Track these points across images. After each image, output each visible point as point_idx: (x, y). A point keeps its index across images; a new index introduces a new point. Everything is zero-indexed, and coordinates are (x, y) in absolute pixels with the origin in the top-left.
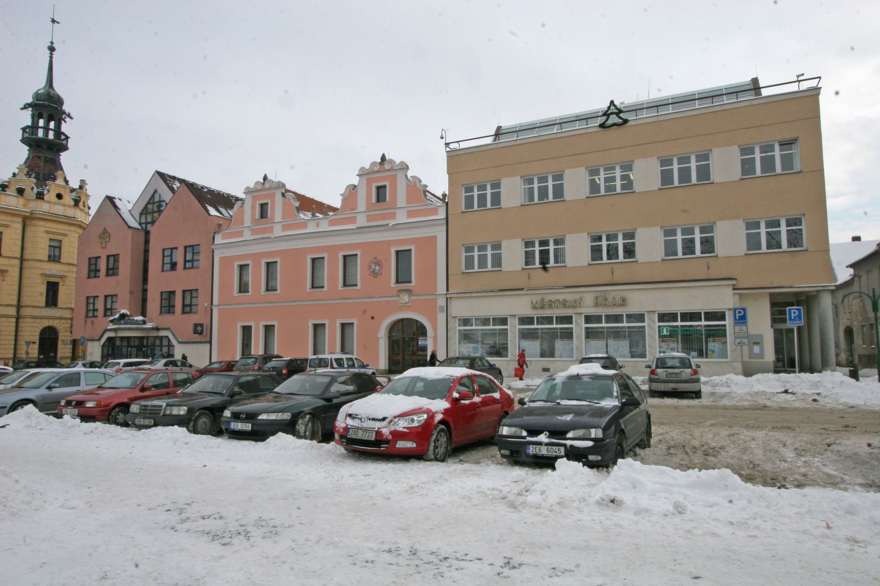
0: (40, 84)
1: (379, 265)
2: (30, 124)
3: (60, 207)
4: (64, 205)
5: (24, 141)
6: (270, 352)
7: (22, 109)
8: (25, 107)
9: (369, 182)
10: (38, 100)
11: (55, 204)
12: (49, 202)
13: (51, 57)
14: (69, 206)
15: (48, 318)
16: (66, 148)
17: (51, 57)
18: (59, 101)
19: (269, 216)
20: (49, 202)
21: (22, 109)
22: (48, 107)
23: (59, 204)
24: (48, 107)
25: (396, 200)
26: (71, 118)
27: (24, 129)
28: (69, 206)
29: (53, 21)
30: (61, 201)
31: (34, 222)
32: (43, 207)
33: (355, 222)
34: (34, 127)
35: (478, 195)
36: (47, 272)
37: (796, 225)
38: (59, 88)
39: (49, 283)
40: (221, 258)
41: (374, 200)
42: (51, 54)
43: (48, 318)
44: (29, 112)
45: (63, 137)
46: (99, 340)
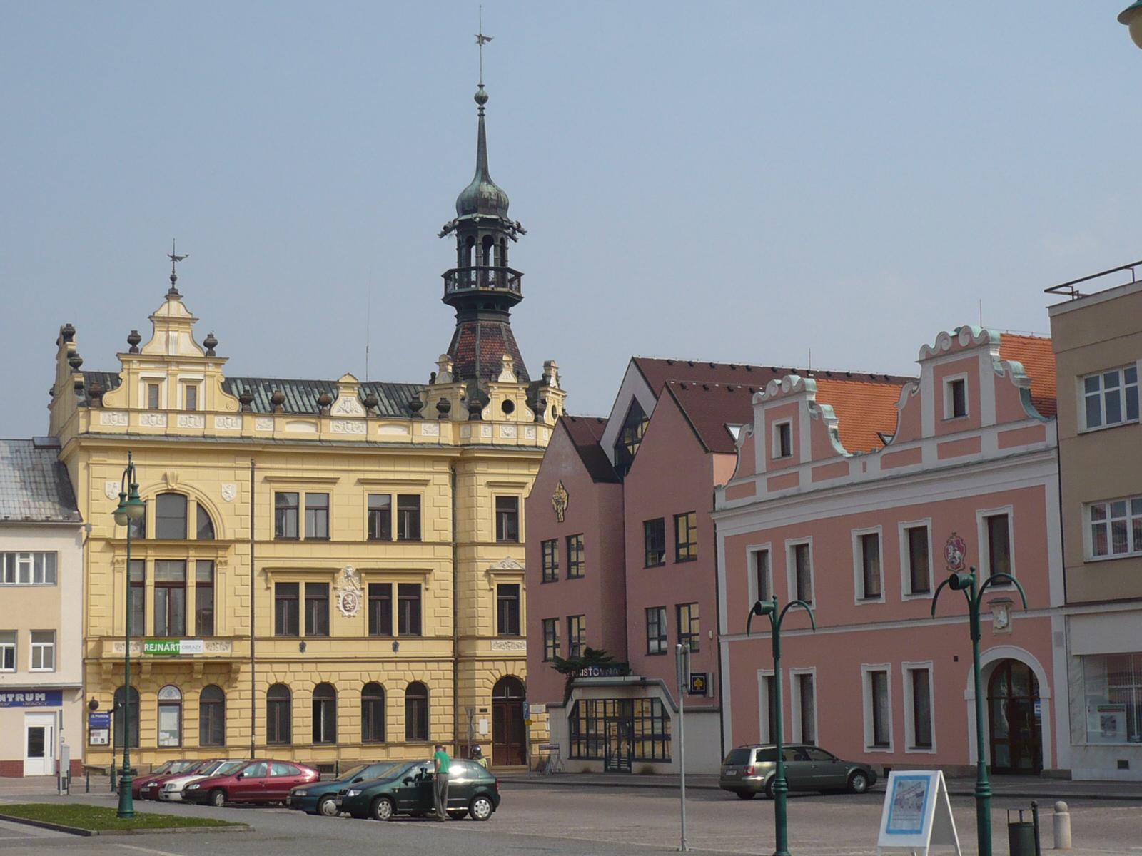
0: (463, 179)
1: (961, 550)
2: (456, 267)
3: (510, 430)
4: (516, 424)
5: (449, 299)
6: (598, 720)
7: (441, 236)
8: (447, 230)
9: (939, 373)
10: (465, 213)
11: (501, 423)
12: (491, 423)
13: (482, 115)
14: (526, 424)
15: (505, 660)
16: (515, 300)
17: (482, 115)
18: (500, 205)
19: (792, 452)
20: (491, 423)
21: (441, 236)
22: (482, 225)
23: (507, 423)
24: (482, 225)
25: (979, 416)
26: (523, 232)
27: (448, 276)
28: (526, 424)
29: (481, 39)
30: (512, 417)
31: (469, 467)
32: (483, 434)
33: (919, 460)
34: (464, 267)
35: (1107, 394)
36: (498, 567)
37: (1124, 532)
38: (503, 179)
39: (502, 589)
40: (726, 538)
41: (948, 411)
42: (482, 109)
43: (505, 660)
44: (452, 240)
45: (510, 276)
46: (564, 706)
